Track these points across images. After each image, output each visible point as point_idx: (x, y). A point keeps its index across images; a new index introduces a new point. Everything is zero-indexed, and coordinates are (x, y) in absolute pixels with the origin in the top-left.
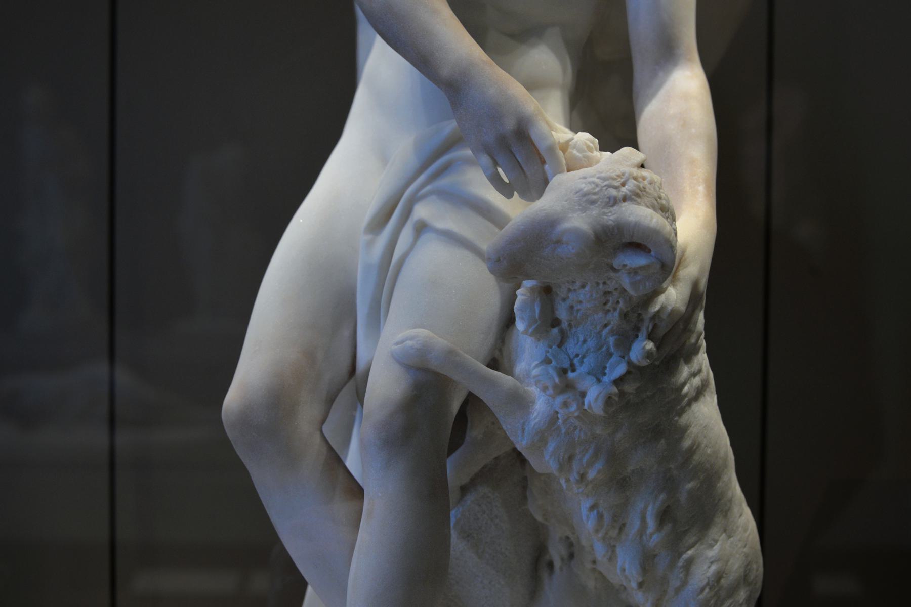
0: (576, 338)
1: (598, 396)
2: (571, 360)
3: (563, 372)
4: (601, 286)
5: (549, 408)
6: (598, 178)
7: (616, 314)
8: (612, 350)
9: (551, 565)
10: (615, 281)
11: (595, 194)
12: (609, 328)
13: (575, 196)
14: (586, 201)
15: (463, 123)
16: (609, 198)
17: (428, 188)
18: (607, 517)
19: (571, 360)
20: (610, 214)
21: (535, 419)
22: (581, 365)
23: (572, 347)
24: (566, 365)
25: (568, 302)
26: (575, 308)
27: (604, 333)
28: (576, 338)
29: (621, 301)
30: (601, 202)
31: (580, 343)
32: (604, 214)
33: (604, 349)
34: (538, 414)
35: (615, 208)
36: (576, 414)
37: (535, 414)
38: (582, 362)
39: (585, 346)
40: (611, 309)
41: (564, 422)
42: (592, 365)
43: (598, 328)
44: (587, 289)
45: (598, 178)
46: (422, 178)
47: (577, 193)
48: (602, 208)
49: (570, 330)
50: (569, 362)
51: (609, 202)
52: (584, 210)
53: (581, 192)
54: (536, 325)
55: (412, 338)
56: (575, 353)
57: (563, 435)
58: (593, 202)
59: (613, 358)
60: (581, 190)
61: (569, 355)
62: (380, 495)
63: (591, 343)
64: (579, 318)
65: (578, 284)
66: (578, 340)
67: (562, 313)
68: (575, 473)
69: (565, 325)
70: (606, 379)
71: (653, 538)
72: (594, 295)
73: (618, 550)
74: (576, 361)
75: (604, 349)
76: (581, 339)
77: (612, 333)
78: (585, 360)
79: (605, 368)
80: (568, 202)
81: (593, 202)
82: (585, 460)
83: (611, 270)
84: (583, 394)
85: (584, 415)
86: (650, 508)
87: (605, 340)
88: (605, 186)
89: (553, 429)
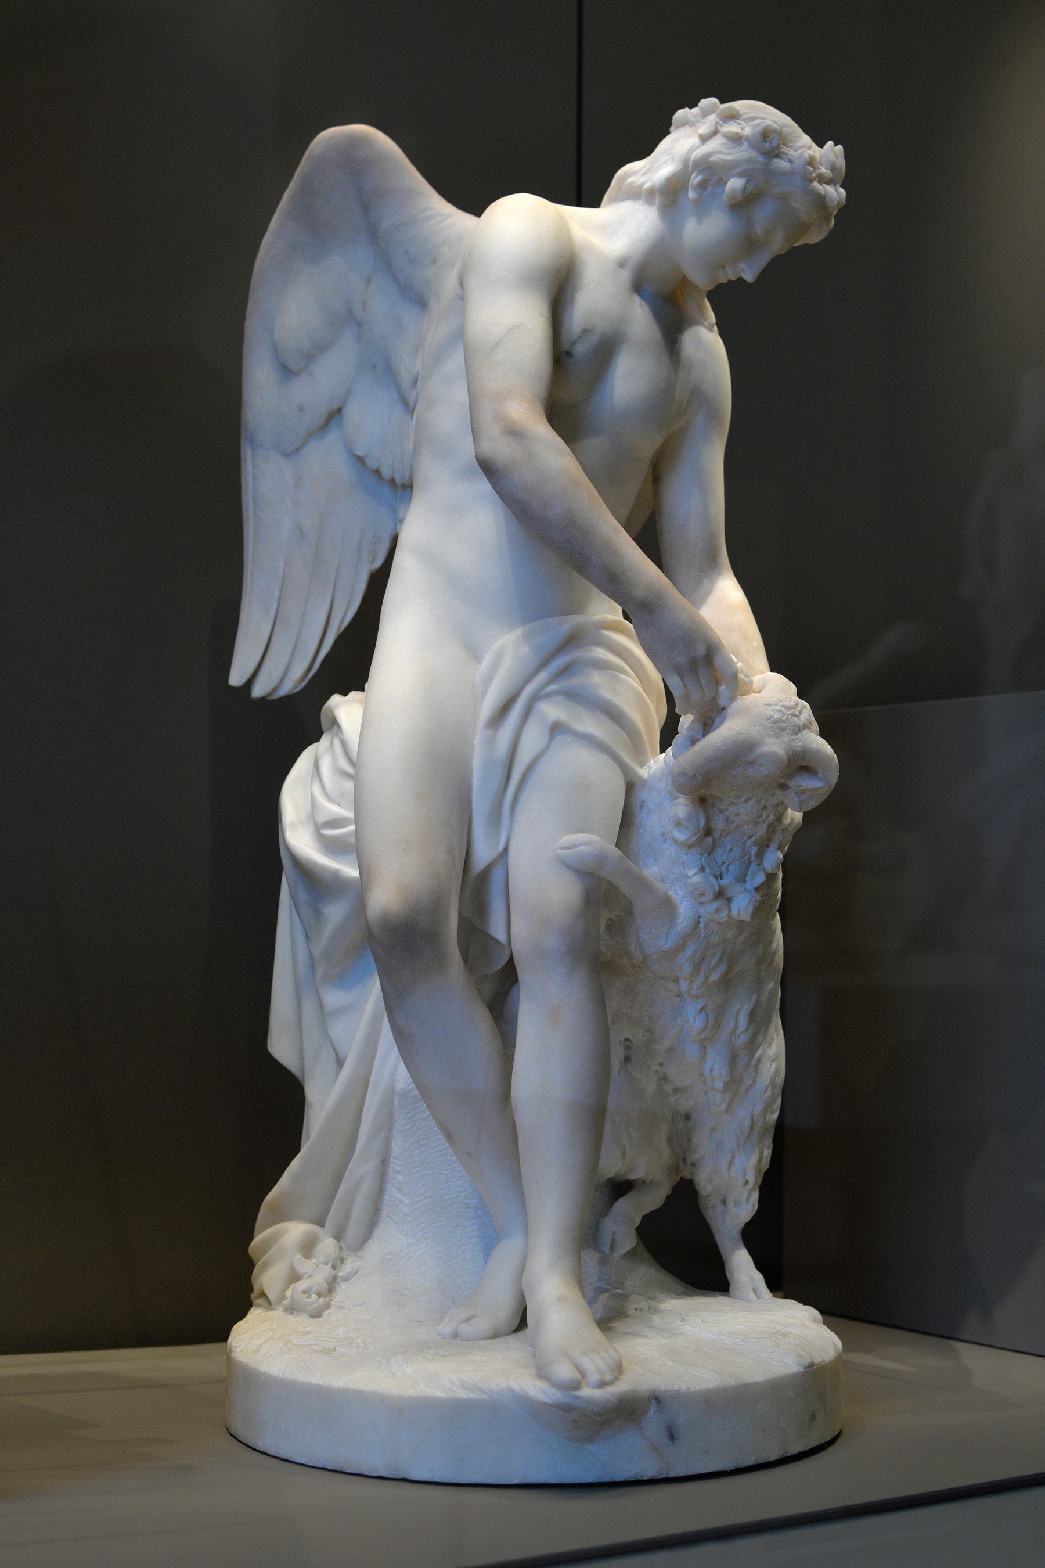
0: (723, 847)
4: (763, 802)
5: (694, 913)
6: (781, 706)
7: (765, 826)
8: (753, 859)
10: (776, 797)
11: (784, 721)
12: (754, 838)
13: (767, 722)
14: (777, 728)
15: (655, 643)
16: (795, 726)
17: (553, 687)
18: (711, 1017)
20: (797, 741)
21: (682, 923)
22: (728, 873)
23: (719, 855)
25: (726, 814)
26: (730, 820)
28: (723, 847)
29: (771, 814)
30: (789, 729)
32: (793, 740)
33: (746, 858)
34: (684, 920)
35: (799, 735)
37: (681, 919)
40: (762, 822)
41: (706, 926)
43: (745, 838)
44: (750, 803)
45: (781, 706)
46: (543, 676)
47: (769, 719)
48: (791, 735)
49: (719, 840)
51: (794, 730)
52: (778, 736)
53: (772, 719)
55: (587, 844)
57: (702, 939)
58: (783, 729)
59: (751, 866)
60: (772, 717)
62: (567, 1001)
63: (737, 853)
64: (732, 828)
65: (744, 798)
67: (719, 824)
68: (702, 976)
69: (716, 835)
70: (748, 886)
71: (740, 1038)
72: (755, 809)
73: (709, 1051)
74: (723, 868)
75: (746, 858)
77: (755, 844)
78: (730, 868)
79: (746, 875)
80: (762, 727)
81: (783, 729)
82: (713, 964)
83: (778, 789)
88: (790, 714)
89: (695, 933)
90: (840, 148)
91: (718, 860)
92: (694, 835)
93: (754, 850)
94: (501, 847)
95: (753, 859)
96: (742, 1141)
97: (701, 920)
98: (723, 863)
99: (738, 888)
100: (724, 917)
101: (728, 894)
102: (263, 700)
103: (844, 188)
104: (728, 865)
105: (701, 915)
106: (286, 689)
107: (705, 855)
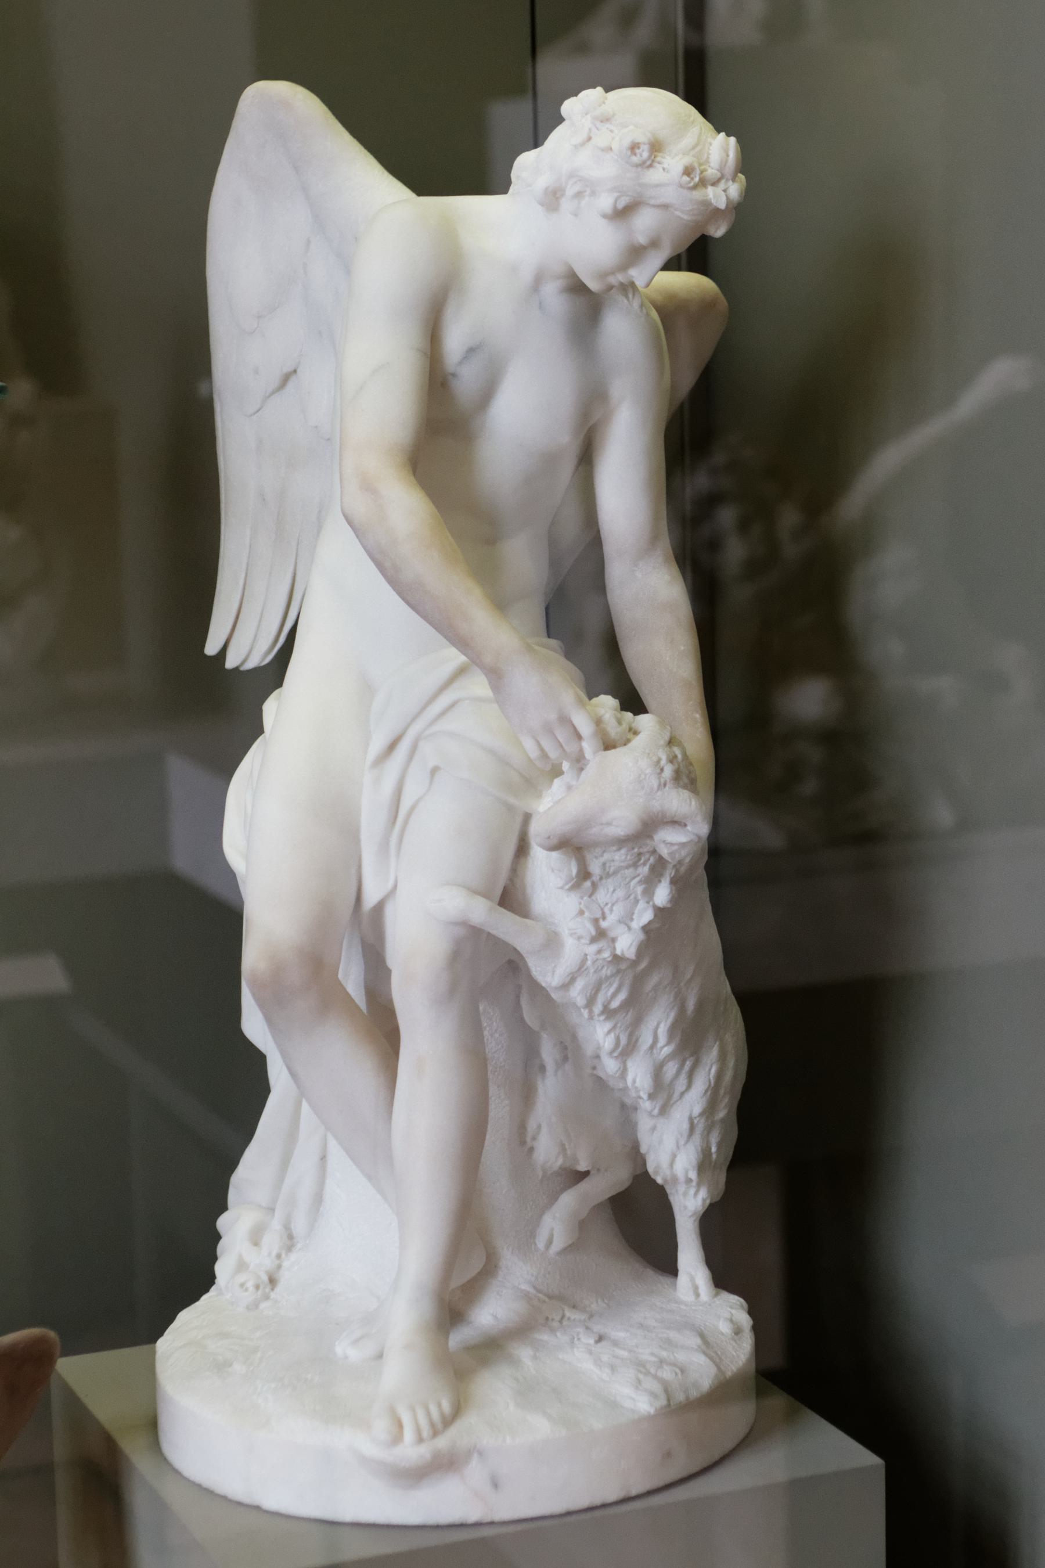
0: (606, 890)
1: (631, 944)
2: (602, 909)
3: (596, 921)
8: (639, 897)
9: (542, 1068)
19: (602, 909)
22: (611, 913)
24: (599, 915)
27: (633, 883)
31: (609, 894)
33: (632, 897)
36: (609, 959)
38: (611, 910)
39: (614, 895)
42: (622, 914)
50: (601, 912)
54: (572, 883)
56: (605, 903)
59: (639, 904)
61: (599, 906)
66: (608, 889)
69: (595, 878)
74: (606, 910)
76: (611, 889)
78: (615, 908)
79: (633, 914)
84: (614, 940)
85: (617, 959)
86: (662, 1025)
87: (633, 889)
90: (733, 140)
91: (600, 901)
92: (567, 883)
93: (639, 889)
94: (390, 885)
95: (639, 897)
96: (682, 1142)
97: (588, 957)
98: (607, 904)
99: (622, 928)
100: (609, 957)
101: (612, 934)
102: (236, 669)
103: (743, 174)
104: (613, 905)
105: (587, 953)
106: (250, 665)
107: (585, 898)
